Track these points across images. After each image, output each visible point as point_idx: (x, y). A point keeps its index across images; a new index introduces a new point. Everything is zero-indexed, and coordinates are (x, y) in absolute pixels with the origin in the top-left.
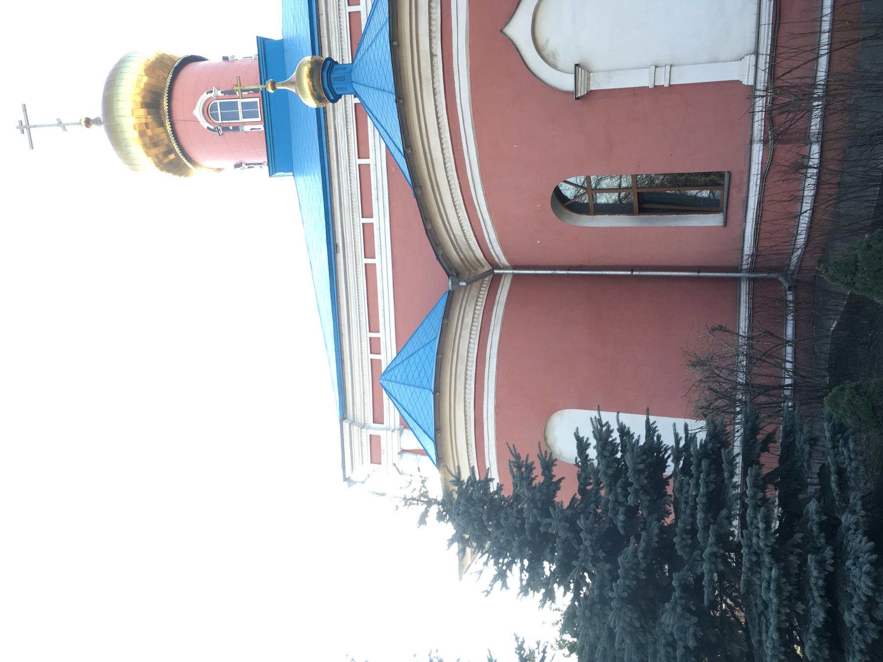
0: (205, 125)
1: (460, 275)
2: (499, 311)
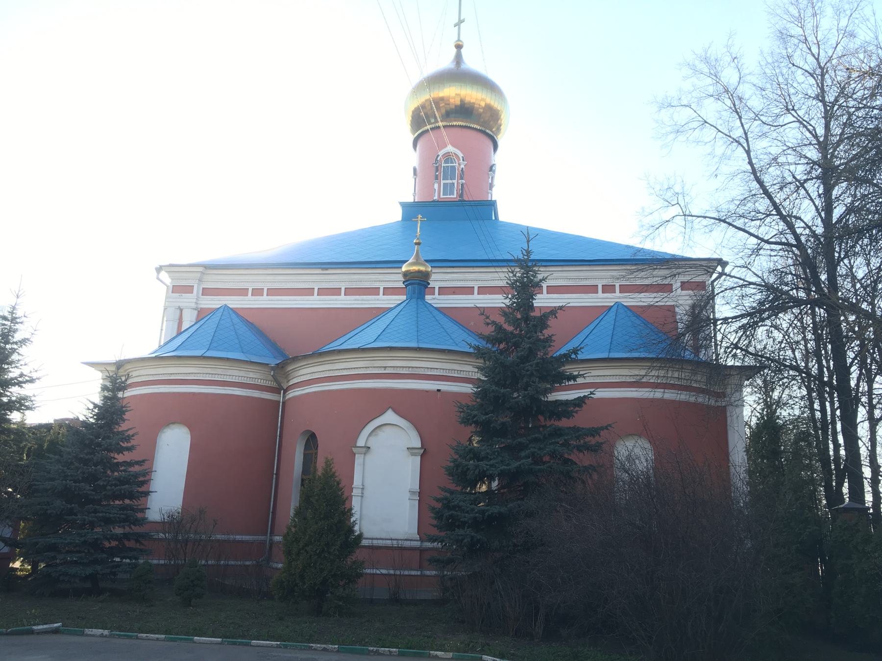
0: (441, 153)
1: (281, 368)
2: (256, 394)
